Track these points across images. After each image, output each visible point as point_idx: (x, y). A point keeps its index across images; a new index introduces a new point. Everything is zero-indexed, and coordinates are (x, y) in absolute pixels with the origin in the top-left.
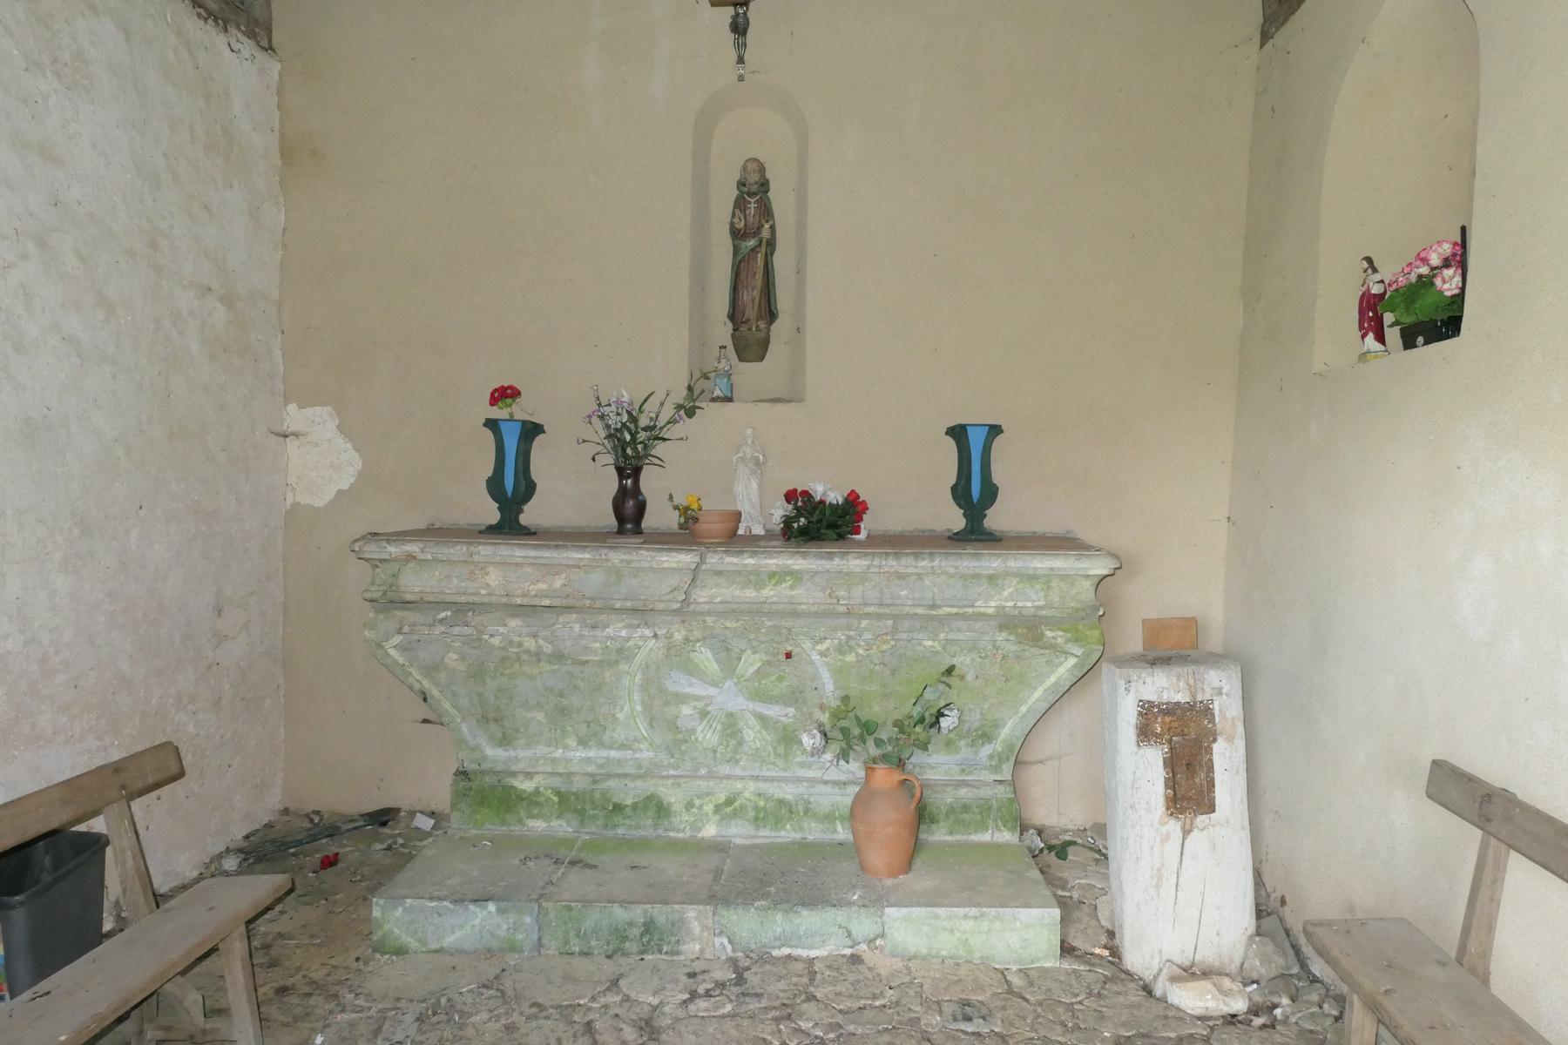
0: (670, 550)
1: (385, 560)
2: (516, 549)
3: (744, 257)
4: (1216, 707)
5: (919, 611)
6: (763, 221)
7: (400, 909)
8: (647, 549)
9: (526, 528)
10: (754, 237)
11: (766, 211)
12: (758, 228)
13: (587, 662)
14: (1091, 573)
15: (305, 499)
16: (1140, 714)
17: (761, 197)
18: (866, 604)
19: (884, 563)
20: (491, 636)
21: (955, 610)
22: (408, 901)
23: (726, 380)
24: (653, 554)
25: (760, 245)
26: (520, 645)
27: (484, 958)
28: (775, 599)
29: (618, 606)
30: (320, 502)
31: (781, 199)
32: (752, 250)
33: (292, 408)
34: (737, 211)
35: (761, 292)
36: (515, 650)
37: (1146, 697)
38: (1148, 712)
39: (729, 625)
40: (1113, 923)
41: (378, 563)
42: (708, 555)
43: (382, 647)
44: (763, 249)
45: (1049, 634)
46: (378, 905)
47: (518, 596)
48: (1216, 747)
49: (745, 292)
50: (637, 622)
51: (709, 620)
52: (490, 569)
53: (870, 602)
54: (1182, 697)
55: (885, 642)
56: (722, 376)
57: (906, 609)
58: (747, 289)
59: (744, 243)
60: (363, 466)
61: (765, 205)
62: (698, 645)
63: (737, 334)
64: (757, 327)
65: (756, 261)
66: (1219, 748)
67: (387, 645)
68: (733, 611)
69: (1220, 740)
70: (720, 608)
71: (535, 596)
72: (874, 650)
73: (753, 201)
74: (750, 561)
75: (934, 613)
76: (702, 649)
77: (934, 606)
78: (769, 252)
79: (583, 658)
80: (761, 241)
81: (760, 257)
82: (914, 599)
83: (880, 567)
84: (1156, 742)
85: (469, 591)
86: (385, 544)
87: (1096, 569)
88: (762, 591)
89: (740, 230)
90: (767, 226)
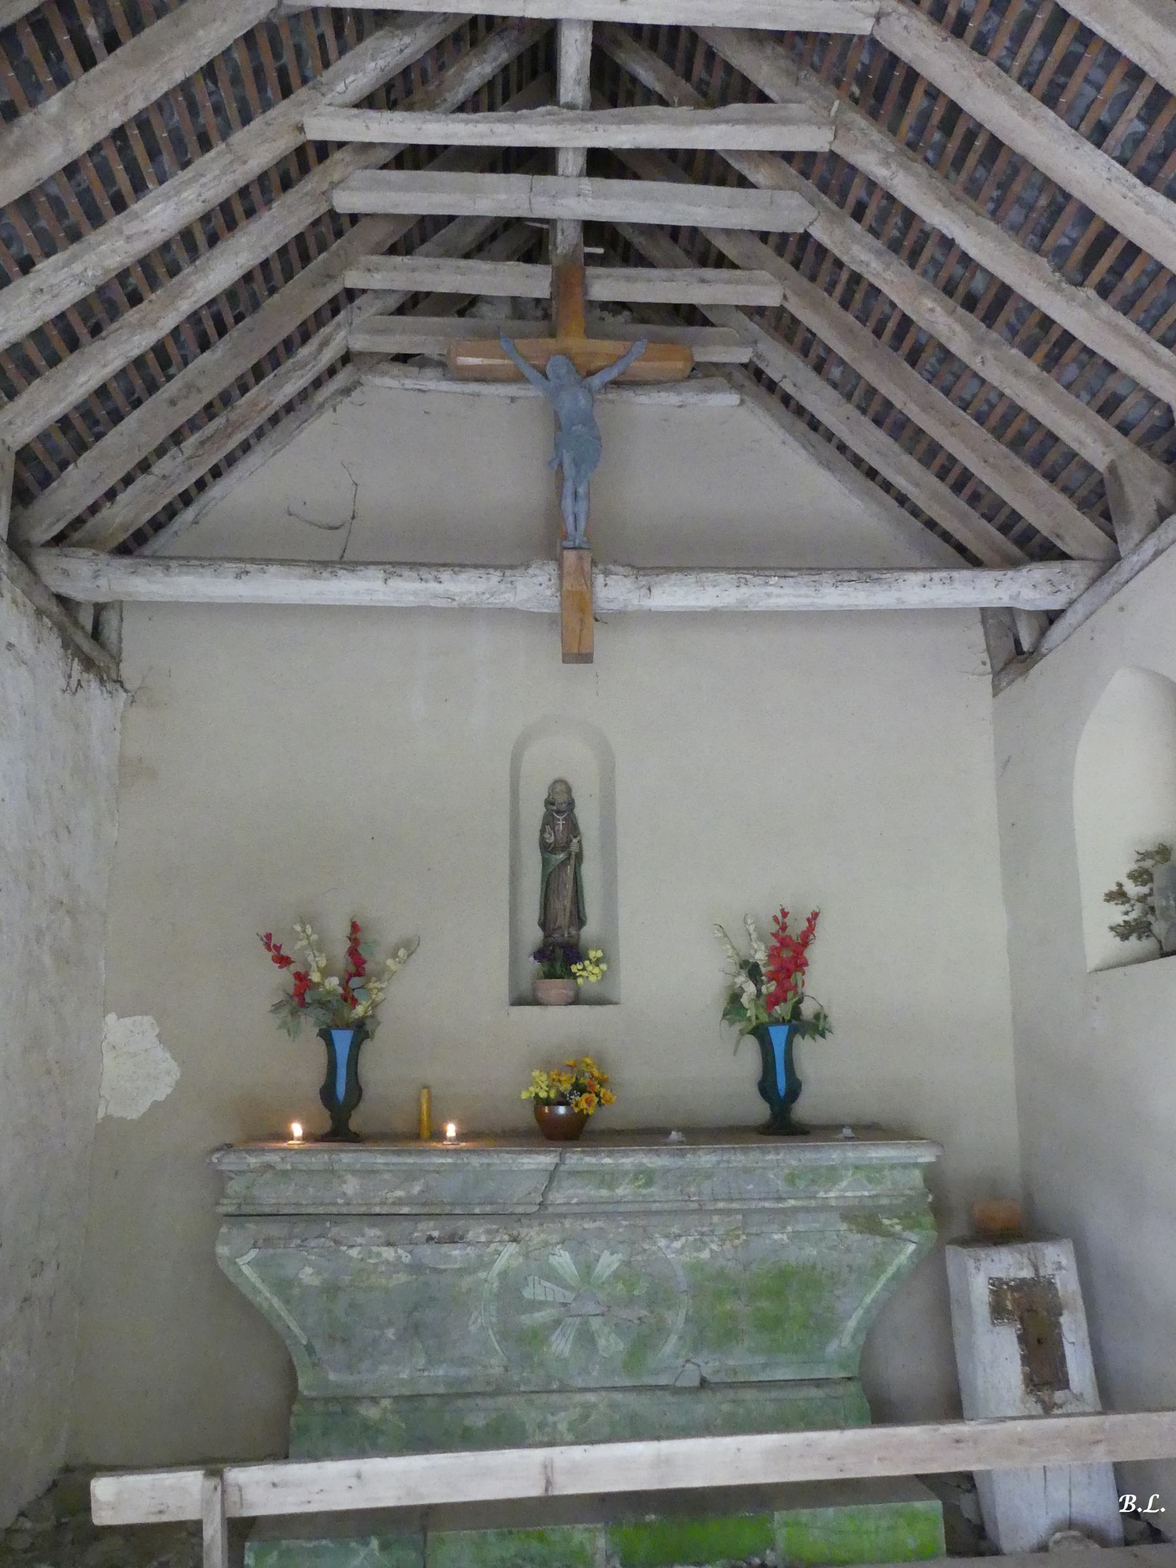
0: (530, 1152)
1: (240, 1172)
2: (379, 1156)
4: (1057, 1282)
5: (767, 1205)
6: (571, 836)
7: (275, 1554)
11: (573, 828)
13: (445, 1270)
14: (920, 1160)
15: (117, 1111)
16: (992, 1291)
18: (716, 1200)
19: (733, 1158)
20: (352, 1246)
21: (799, 1203)
22: (284, 1542)
24: (514, 1156)
25: (568, 858)
26: (379, 1255)
29: (477, 1211)
30: (133, 1114)
31: (587, 816)
33: (111, 1018)
34: (548, 828)
36: (372, 1261)
37: (994, 1275)
38: (998, 1288)
39: (586, 1226)
40: (981, 1516)
41: (233, 1175)
42: (567, 1155)
43: (235, 1263)
44: (572, 861)
45: (886, 1222)
46: (250, 1549)
47: (375, 1205)
48: (1062, 1320)
50: (495, 1227)
52: (349, 1177)
53: (719, 1197)
54: (1027, 1273)
55: (738, 1237)
60: (181, 1076)
62: (559, 1247)
64: (569, 933)
65: (566, 874)
66: (1064, 1320)
67: (240, 1261)
68: (589, 1211)
69: (1065, 1312)
70: (577, 1209)
71: (394, 1204)
72: (728, 1245)
73: (561, 818)
74: (608, 1160)
75: (781, 1205)
76: (562, 1252)
79: (442, 1267)
80: (570, 854)
81: (569, 870)
83: (729, 1162)
84: (1008, 1319)
85: (326, 1201)
86: (244, 1155)
87: (925, 1156)
88: (617, 1191)
90: (575, 841)
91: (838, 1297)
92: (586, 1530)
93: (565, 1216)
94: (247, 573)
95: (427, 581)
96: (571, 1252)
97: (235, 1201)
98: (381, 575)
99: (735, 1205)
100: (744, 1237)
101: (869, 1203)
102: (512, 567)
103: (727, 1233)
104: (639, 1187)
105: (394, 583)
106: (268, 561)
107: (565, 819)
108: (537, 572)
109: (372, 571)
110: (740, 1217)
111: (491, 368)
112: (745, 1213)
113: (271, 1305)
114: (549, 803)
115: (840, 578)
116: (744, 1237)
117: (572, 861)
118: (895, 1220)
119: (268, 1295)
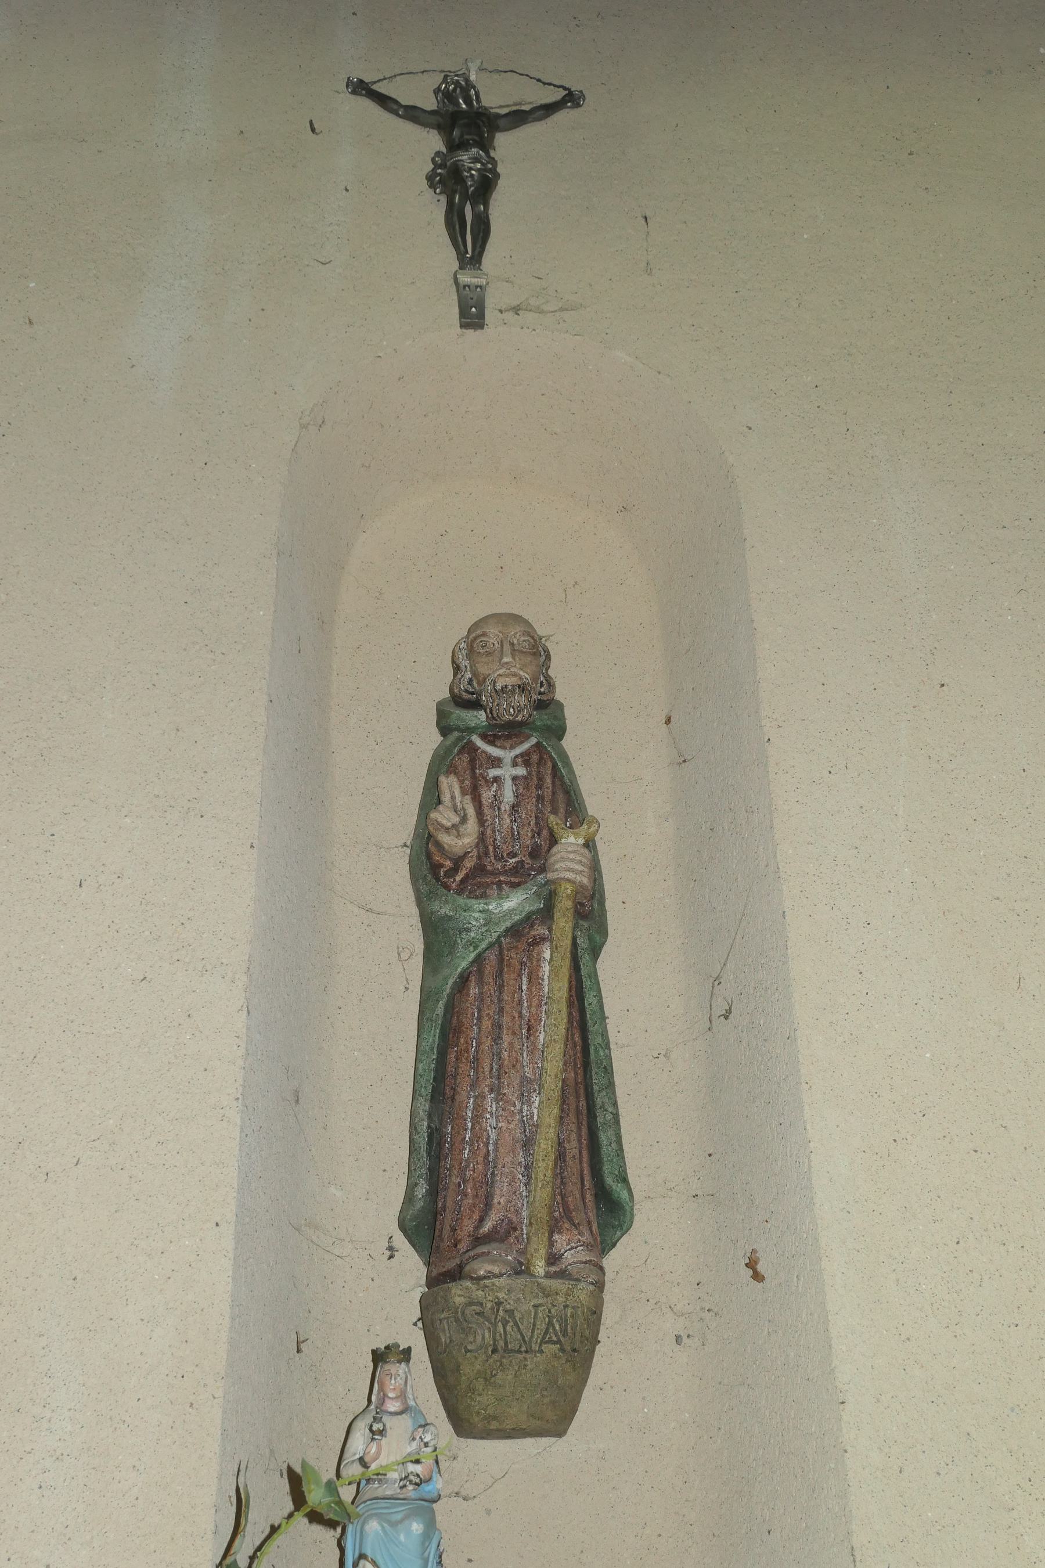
3: (479, 960)
12: (535, 853)
17: (538, 745)
23: (417, 1527)
25: (547, 913)
27: (535, 1358)
32: (515, 932)
34: (449, 785)
35: (564, 1100)
44: (563, 923)
49: (490, 1104)
56: (398, 1512)
58: (497, 1090)
59: (478, 905)
61: (555, 768)
63: (458, 1293)
64: (553, 1259)
65: (534, 979)
73: (507, 755)
78: (582, 942)
107: (525, 759)
111: (242, 1501)
117: (563, 923)
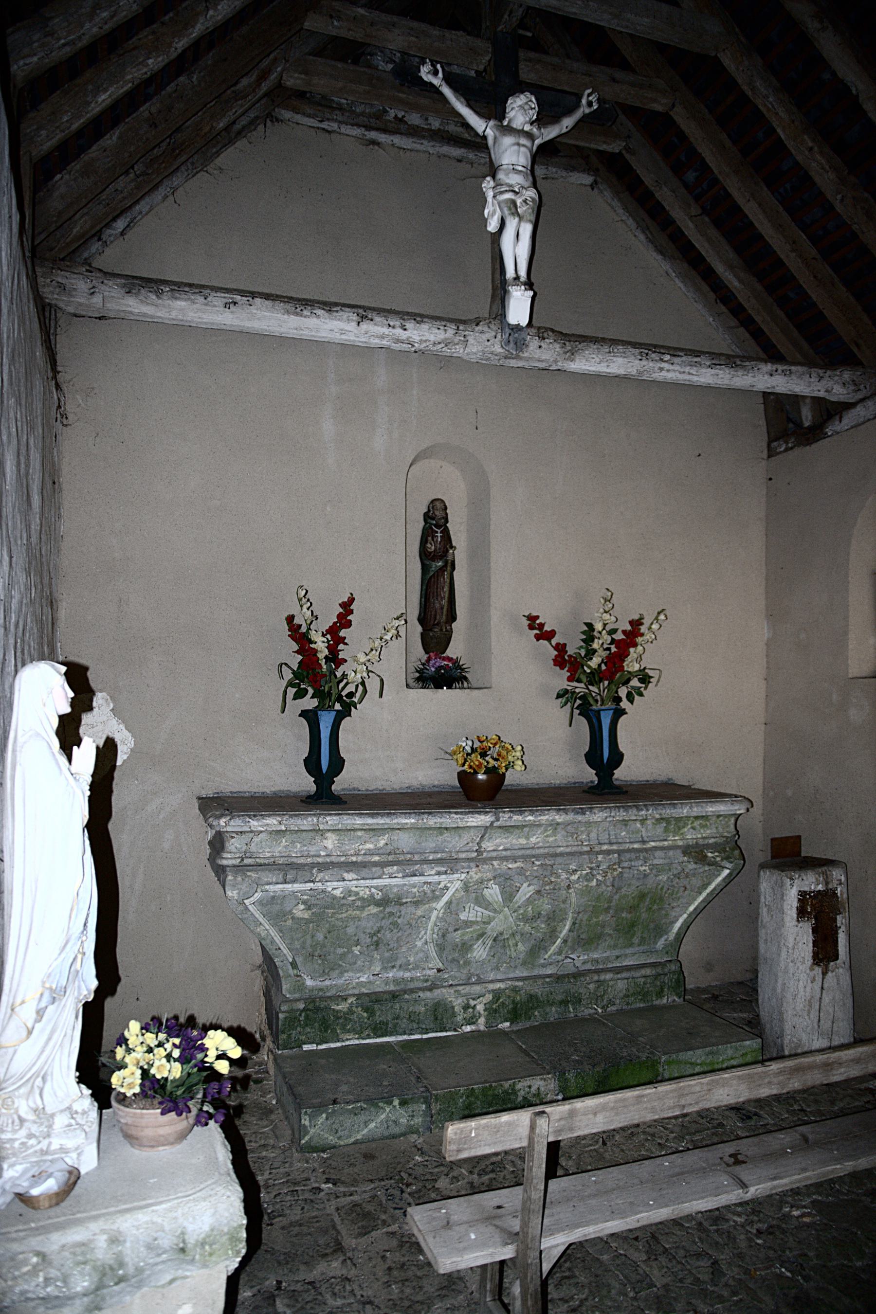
5: (636, 846)
7: (324, 1115)
8: (456, 813)
9: (618, 787)
10: (441, 559)
13: (406, 903)
24: (462, 816)
25: (445, 566)
28: (541, 844)
32: (440, 569)
39: (510, 866)
44: (449, 568)
51: (495, 863)
55: (615, 870)
57: (627, 846)
71: (365, 854)
74: (531, 818)
77: (644, 842)
82: (630, 838)
85: (312, 853)
89: (431, 553)
91: (673, 908)
92: (541, 1079)
93: (492, 859)
94: (235, 303)
95: (394, 327)
96: (500, 886)
97: (237, 856)
98: (355, 317)
99: (615, 847)
100: (620, 870)
101: (701, 842)
102: (464, 322)
103: (609, 867)
104: (547, 836)
105: (365, 326)
106: (253, 295)
108: (486, 329)
109: (348, 314)
110: (616, 855)
112: (620, 852)
113: (269, 934)
114: (427, 517)
115: (714, 362)
116: (620, 870)
117: (449, 568)
118: (716, 854)
119: (268, 927)
